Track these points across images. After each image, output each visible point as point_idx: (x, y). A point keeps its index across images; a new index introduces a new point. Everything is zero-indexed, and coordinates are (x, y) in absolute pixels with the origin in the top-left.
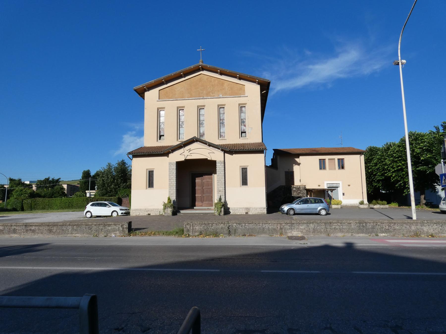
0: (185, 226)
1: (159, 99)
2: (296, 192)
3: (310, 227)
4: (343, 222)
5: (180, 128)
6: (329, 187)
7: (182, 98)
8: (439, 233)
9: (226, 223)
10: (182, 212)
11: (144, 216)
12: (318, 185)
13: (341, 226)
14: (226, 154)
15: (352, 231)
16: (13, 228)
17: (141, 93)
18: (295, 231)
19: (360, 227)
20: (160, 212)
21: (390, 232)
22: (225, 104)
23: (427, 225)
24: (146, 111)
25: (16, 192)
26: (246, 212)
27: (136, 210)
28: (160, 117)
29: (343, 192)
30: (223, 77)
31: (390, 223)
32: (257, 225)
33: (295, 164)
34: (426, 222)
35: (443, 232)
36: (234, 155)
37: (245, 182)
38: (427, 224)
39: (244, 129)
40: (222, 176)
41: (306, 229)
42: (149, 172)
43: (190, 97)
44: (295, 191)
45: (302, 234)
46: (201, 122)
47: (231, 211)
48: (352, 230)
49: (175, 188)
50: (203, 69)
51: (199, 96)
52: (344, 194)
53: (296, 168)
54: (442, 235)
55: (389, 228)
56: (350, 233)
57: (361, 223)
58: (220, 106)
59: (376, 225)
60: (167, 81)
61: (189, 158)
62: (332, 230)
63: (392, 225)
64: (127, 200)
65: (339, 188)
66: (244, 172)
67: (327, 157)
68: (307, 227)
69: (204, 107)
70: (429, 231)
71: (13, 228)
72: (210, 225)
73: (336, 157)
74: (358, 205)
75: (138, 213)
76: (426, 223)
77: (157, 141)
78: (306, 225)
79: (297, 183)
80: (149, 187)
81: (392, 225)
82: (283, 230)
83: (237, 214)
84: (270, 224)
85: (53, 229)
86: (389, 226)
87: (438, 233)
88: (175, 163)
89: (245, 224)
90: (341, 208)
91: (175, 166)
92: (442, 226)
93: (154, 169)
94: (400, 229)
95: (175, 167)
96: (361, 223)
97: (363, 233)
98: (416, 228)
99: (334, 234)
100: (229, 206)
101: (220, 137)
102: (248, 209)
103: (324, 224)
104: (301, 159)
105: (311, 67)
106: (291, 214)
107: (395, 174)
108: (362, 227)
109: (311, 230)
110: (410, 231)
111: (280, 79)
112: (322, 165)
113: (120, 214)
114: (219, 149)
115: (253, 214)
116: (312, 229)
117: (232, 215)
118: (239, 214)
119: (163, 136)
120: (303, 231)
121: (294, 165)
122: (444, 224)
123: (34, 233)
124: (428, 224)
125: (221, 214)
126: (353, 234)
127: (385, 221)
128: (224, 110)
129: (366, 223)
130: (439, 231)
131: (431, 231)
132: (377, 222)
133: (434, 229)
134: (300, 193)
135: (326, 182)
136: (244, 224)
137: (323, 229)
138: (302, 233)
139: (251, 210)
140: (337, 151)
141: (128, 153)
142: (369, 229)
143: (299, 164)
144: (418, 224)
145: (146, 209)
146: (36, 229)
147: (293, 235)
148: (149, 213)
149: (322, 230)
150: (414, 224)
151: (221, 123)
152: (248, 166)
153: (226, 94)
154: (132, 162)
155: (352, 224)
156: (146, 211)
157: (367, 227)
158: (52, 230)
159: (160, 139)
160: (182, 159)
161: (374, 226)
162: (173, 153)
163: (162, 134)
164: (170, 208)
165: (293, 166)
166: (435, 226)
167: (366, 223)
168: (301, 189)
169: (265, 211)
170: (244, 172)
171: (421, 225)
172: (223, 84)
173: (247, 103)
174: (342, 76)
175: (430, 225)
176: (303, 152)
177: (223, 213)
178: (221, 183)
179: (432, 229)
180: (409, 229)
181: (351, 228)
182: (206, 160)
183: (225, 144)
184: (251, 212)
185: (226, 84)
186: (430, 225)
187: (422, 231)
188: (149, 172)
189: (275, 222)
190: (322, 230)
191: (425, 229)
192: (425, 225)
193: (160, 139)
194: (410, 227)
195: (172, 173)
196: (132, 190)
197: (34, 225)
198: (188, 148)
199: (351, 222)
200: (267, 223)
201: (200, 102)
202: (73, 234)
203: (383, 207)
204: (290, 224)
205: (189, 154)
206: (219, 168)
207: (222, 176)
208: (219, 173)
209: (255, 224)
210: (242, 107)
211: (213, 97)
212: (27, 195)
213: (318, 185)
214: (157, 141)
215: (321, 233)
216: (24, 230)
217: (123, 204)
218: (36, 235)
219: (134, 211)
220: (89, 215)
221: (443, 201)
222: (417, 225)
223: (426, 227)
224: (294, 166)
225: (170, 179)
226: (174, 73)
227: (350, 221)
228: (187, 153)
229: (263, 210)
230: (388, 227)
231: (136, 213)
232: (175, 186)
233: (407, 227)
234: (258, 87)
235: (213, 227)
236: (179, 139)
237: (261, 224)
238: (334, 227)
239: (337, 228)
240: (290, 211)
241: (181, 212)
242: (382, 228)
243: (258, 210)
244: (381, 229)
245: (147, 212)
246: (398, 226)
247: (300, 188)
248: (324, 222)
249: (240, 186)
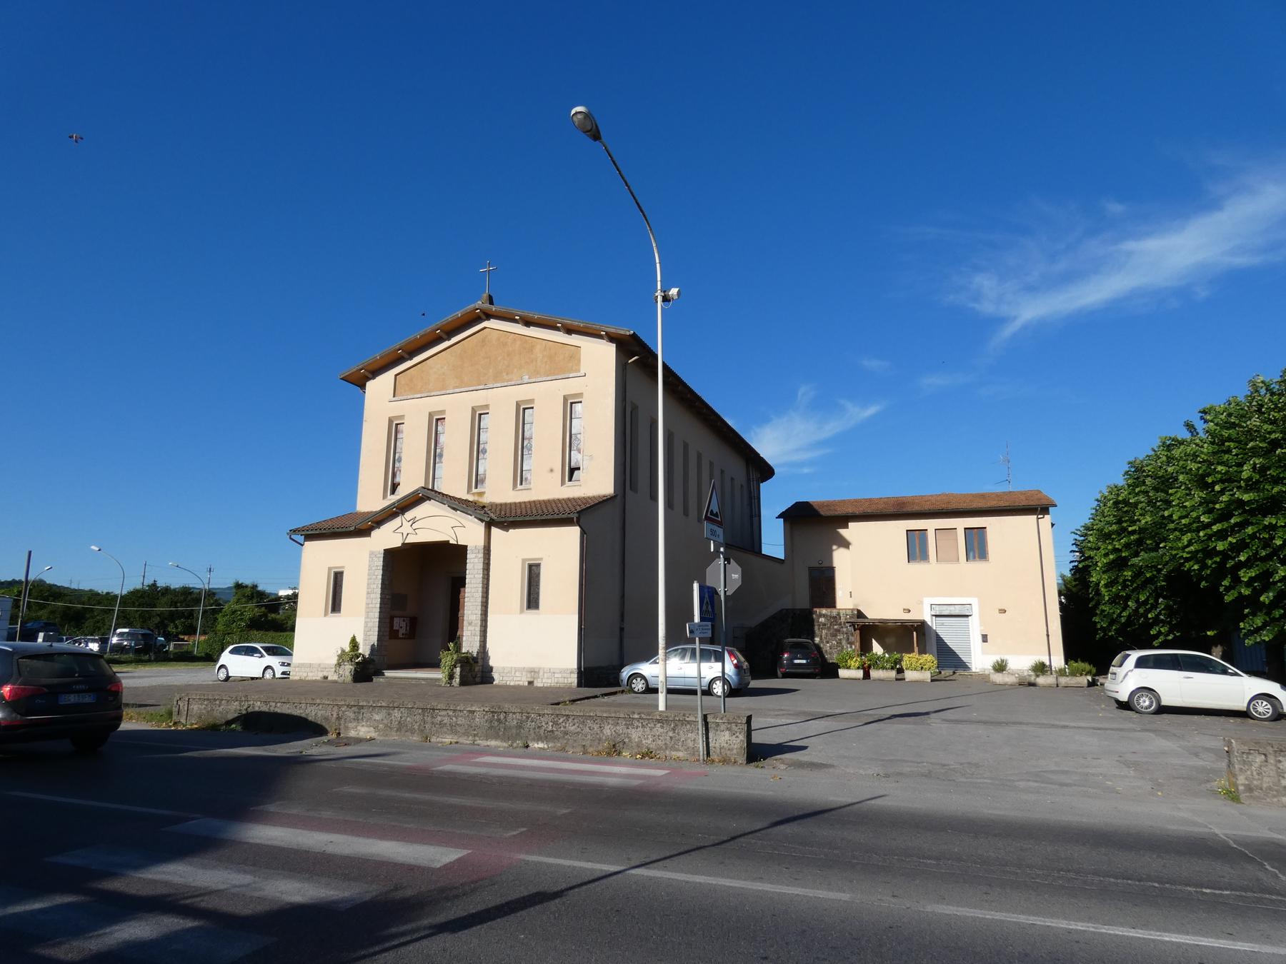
0: (175, 703)
1: (394, 396)
2: (829, 629)
3: (393, 717)
4: (458, 708)
5: (437, 465)
6: (938, 614)
7: (443, 390)
8: (666, 748)
9: (243, 699)
10: (388, 673)
11: (315, 681)
12: (1000, 610)
13: (454, 718)
14: (494, 530)
15: (475, 732)
17: (359, 381)
18: (363, 726)
19: (491, 722)
21: (556, 738)
23: (640, 725)
24: (365, 426)
25: (224, 616)
26: (529, 680)
27: (301, 666)
28: (571, 418)
29: (981, 630)
31: (557, 715)
32: (296, 707)
33: (836, 544)
34: (636, 716)
35: (677, 746)
36: (511, 531)
37: (532, 601)
38: (641, 721)
39: (577, 461)
40: (477, 585)
41: (385, 722)
42: (530, 566)
43: (457, 387)
44: (824, 625)
45: (377, 733)
46: (481, 447)
47: (495, 675)
48: (475, 730)
49: (377, 615)
50: (488, 316)
51: (480, 383)
52: (985, 638)
53: (840, 559)
54: (673, 753)
55: (555, 729)
56: (471, 737)
57: (495, 712)
58: (396, 420)
59: (528, 718)
60: (412, 353)
61: (411, 540)
62: (435, 727)
63: (561, 721)
65: (970, 617)
66: (533, 574)
67: (930, 525)
68: (388, 717)
69: (404, 419)
70: (644, 742)
72: (218, 702)
73: (961, 524)
74: (987, 672)
75: (305, 674)
76: (638, 720)
77: (384, 498)
78: (384, 711)
79: (844, 601)
80: (529, 607)
81: (561, 721)
82: (343, 721)
83: (508, 683)
84: (321, 706)
86: (555, 723)
87: (664, 747)
88: (383, 552)
89: (276, 703)
90: (932, 681)
91: (382, 559)
92: (674, 730)
93: (541, 559)
94: (577, 733)
95: (380, 563)
96: (495, 712)
97: (496, 737)
98: (615, 731)
99: (438, 737)
100: (491, 663)
101: (567, 479)
102: (535, 672)
103: (420, 711)
104: (853, 531)
105: (1130, 245)
106: (636, 690)
107: (1107, 577)
108: (496, 723)
109: (395, 724)
110: (600, 740)
111: (1031, 289)
112: (916, 548)
113: (278, 675)
115: (545, 685)
116: (397, 723)
117: (497, 686)
118: (512, 684)
119: (579, 469)
120: (378, 727)
121: (834, 547)
122: (679, 724)
124: (642, 723)
125: (454, 684)
126: (477, 738)
127: (546, 711)
128: (532, 415)
129: (505, 713)
130: (666, 744)
131: (648, 742)
132: (529, 711)
133: (654, 736)
134: (838, 631)
135: (928, 601)
136: (274, 704)
137: (418, 724)
138: (375, 732)
139: (541, 674)
140: (953, 506)
141: (291, 531)
142: (510, 728)
143: (846, 544)
144: (619, 722)
145: (320, 665)
147: (358, 734)
148: (325, 674)
149: (416, 727)
150: (610, 721)
151: (477, 450)
153: (537, 373)
154: (303, 551)
155: (477, 714)
156: (319, 670)
157: (507, 723)
159: (570, 479)
160: (396, 543)
161: (522, 722)
162: (379, 528)
163: (573, 465)
164: (350, 663)
165: (831, 551)
166: (658, 729)
167: (505, 713)
168: (843, 620)
169: (573, 679)
170: (533, 574)
171: (625, 725)
172: (531, 350)
175: (647, 724)
176: (857, 511)
177: (458, 680)
178: (474, 603)
179: (649, 737)
180: (597, 734)
181: (473, 725)
182: (446, 543)
183: (526, 500)
184: (539, 680)
185: (538, 348)
186: (647, 724)
187: (626, 740)
188: (530, 566)
189: (328, 703)
190: (416, 727)
191: (635, 734)
192: (636, 723)
193: (570, 479)
194: (600, 727)
195: (374, 577)
196: (297, 619)
198: (409, 515)
199: (473, 709)
200: (315, 704)
201: (478, 398)
203: (1069, 682)
204: (356, 708)
205: (410, 530)
206: (472, 565)
207: (477, 585)
208: (472, 576)
209: (294, 703)
210: (570, 404)
211: (506, 384)
212: (243, 624)
213: (1000, 610)
214: (563, 483)
215: (412, 732)
219: (297, 669)
220: (222, 675)
222: (618, 723)
223: (638, 730)
224: (835, 550)
225: (368, 593)
226: (422, 332)
227: (472, 705)
228: (407, 528)
229: (568, 675)
230: (552, 726)
231: (301, 673)
232: (378, 610)
233: (594, 728)
234: (612, 348)
235: (222, 707)
236: (521, 484)
237: (303, 705)
238: (439, 720)
239: (445, 721)
240: (634, 681)
241: (386, 674)
242: (539, 727)
243: (556, 675)
244: (537, 730)
245: (322, 671)
246: (574, 725)
247: (840, 617)
248: (421, 705)
249: (522, 611)
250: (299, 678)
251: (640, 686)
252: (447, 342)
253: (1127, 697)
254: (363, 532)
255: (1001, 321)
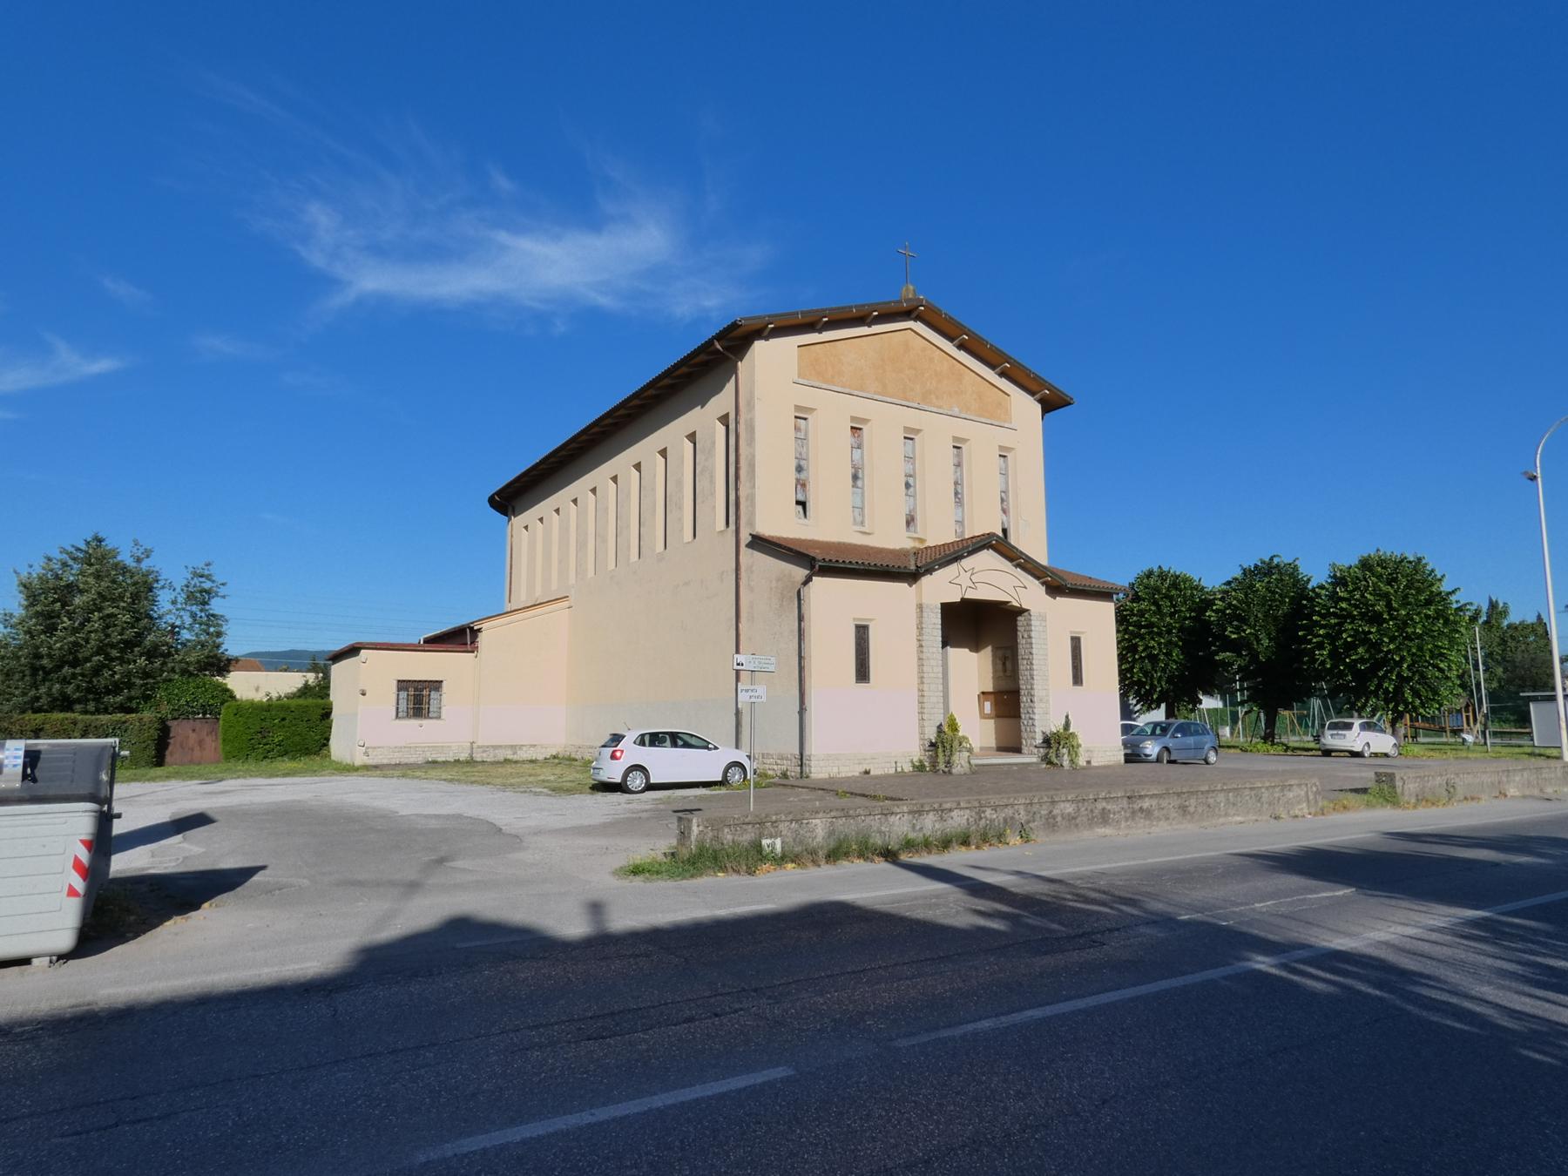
16: (1101, 805)
20: (896, 763)
22: (967, 437)
30: (963, 356)
42: (858, 627)
43: (879, 394)
64: (194, 730)
71: (1101, 805)
75: (835, 770)
85: (1190, 805)
91: (939, 616)
105: (503, 236)
111: (379, 252)
114: (1038, 578)
123: (1150, 819)
146: (1153, 807)
152: (871, 620)
158: (1187, 807)
173: (816, 409)
174: (604, 301)
197: (1146, 796)
202: (1229, 815)
216: (1125, 812)
217: (170, 748)
218: (1154, 825)
219: (822, 763)
221: (1328, 729)
243: (1108, 753)
245: (859, 764)
250: (827, 776)
251: (638, 782)
252: (866, 328)
253: (721, 775)
254: (912, 577)
255: (330, 283)
